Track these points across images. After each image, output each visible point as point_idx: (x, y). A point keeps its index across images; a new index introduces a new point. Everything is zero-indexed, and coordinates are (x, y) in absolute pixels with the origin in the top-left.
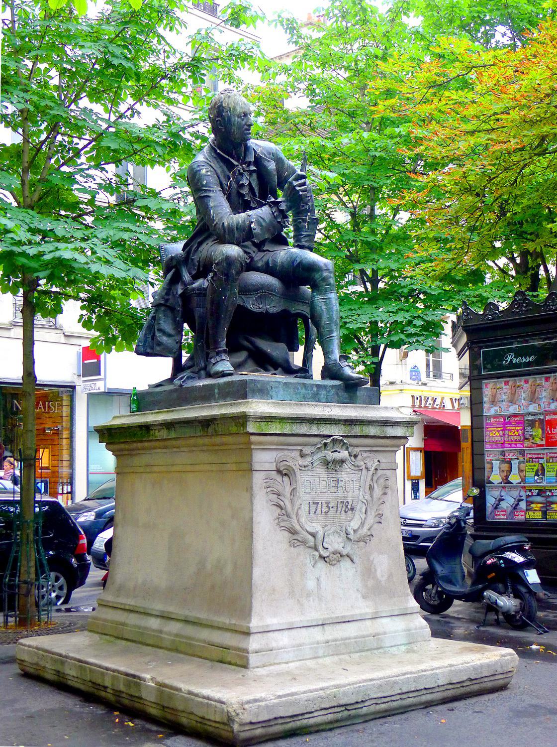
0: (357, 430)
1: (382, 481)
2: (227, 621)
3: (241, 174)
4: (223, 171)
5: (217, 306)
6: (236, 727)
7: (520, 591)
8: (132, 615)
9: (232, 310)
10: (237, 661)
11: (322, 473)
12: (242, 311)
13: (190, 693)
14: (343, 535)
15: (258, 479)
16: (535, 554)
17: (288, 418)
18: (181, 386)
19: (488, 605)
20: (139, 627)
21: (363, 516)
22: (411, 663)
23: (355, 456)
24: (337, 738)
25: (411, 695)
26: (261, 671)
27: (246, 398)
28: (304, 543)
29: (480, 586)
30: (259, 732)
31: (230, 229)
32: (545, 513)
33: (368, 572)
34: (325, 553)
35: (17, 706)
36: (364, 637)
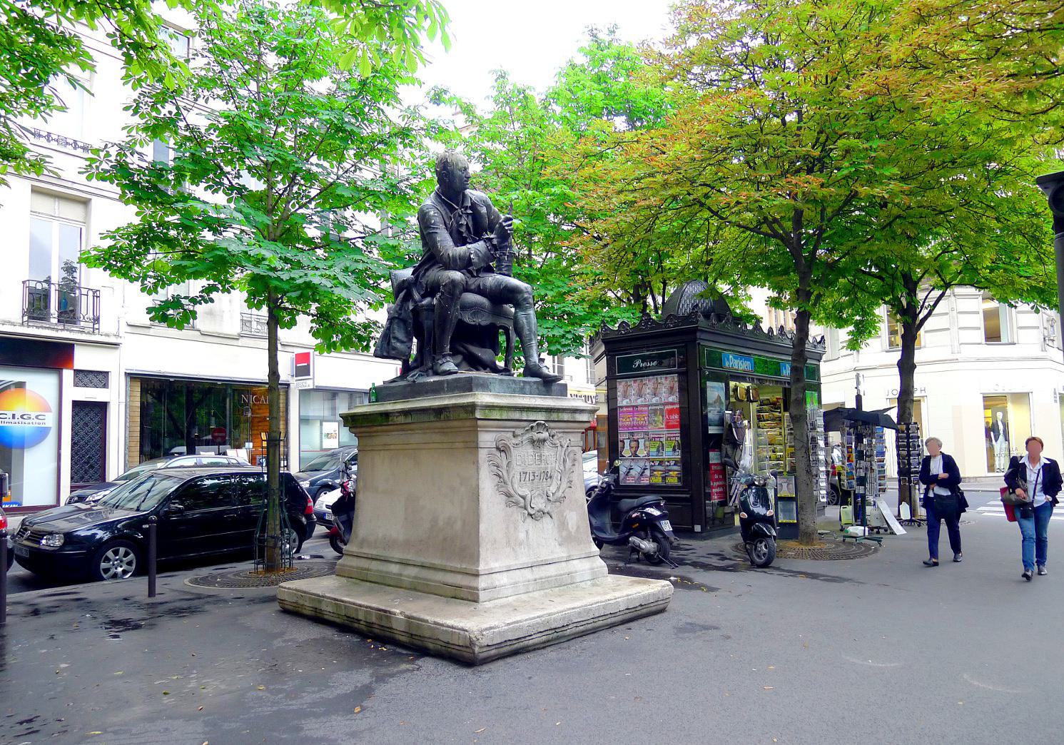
0: (554, 416)
1: (572, 455)
2: (459, 566)
3: (461, 216)
4: (446, 213)
5: (444, 319)
6: (477, 649)
7: (657, 537)
8: (374, 562)
9: (455, 321)
10: (471, 597)
11: (530, 450)
12: (461, 323)
13: (436, 623)
14: (545, 497)
15: (483, 454)
16: (667, 510)
17: (505, 407)
18: (414, 381)
19: (632, 547)
20: (381, 572)
21: (559, 482)
22: (599, 594)
23: (553, 436)
24: (550, 654)
25: (600, 619)
26: (488, 605)
27: (471, 391)
28: (517, 503)
29: (627, 534)
30: (493, 652)
31: (454, 258)
32: (664, 478)
33: (563, 525)
34: (532, 512)
35: (286, 637)
36: (561, 575)
